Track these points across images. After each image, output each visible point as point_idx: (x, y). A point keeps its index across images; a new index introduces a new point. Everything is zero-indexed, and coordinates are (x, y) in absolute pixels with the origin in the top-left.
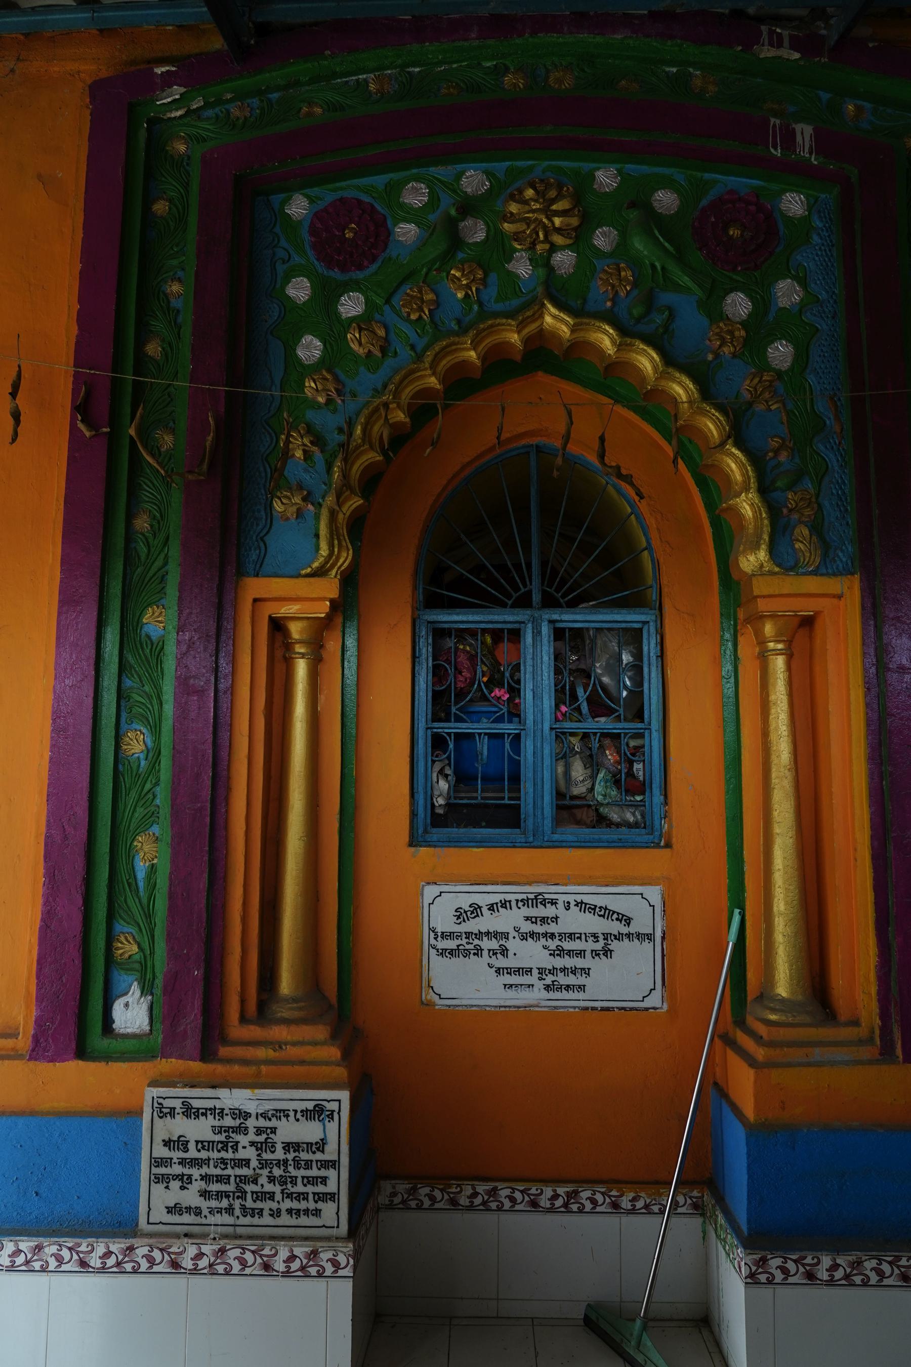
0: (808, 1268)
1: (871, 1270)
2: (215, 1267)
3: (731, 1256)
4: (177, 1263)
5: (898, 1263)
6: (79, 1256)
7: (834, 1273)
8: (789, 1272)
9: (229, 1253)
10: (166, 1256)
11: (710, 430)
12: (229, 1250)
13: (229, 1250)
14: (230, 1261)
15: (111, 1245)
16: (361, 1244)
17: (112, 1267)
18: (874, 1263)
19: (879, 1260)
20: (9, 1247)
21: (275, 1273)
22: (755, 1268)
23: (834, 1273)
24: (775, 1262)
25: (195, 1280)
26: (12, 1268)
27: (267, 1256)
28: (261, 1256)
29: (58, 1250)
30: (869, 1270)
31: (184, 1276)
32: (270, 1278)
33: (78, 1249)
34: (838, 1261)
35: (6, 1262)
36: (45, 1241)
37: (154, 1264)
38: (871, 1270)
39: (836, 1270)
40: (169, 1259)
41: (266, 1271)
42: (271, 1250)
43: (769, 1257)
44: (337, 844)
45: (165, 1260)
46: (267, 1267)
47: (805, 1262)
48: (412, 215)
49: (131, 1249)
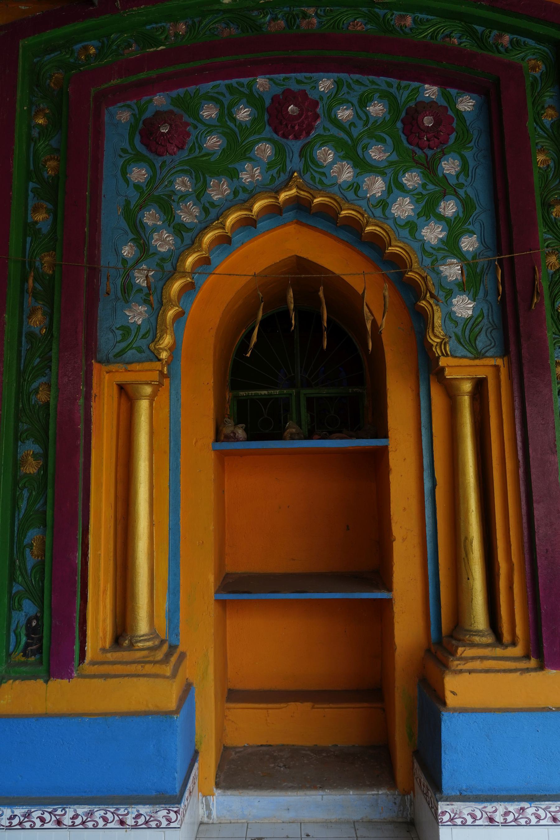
0: (121, 817)
1: (468, 815)
2: (519, 820)
3: (430, 805)
4: (493, 819)
5: (55, 813)
6: (56, 818)
7: (506, 817)
8: (108, 820)
9: (527, 810)
10: (548, 814)
11: (208, 239)
12: (33, 812)
13: (33, 812)
14: (34, 820)
15: (77, 809)
16: (186, 804)
17: (447, 822)
18: (102, 813)
19: (105, 810)
20: (8, 812)
21: (497, 824)
22: (23, 818)
23: (12, 821)
24: (36, 814)
25: (73, 832)
26: (10, 827)
27: (59, 815)
28: (55, 815)
29: (41, 814)
30: (98, 818)
31: (67, 830)
32: (494, 827)
33: (55, 813)
34: (141, 812)
35: (5, 822)
36: (95, 808)
37: (171, 822)
38: (468, 815)
39: (508, 815)
40: (56, 819)
41: (59, 825)
42: (62, 811)
43: (95, 810)
44: (437, 511)
45: (548, 817)
46: (59, 822)
47: (550, 810)
48: (210, 129)
49: (523, 809)
